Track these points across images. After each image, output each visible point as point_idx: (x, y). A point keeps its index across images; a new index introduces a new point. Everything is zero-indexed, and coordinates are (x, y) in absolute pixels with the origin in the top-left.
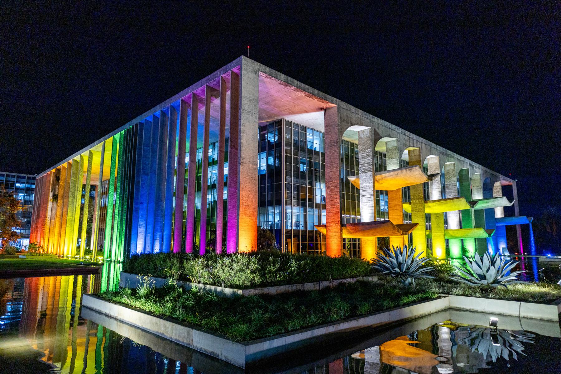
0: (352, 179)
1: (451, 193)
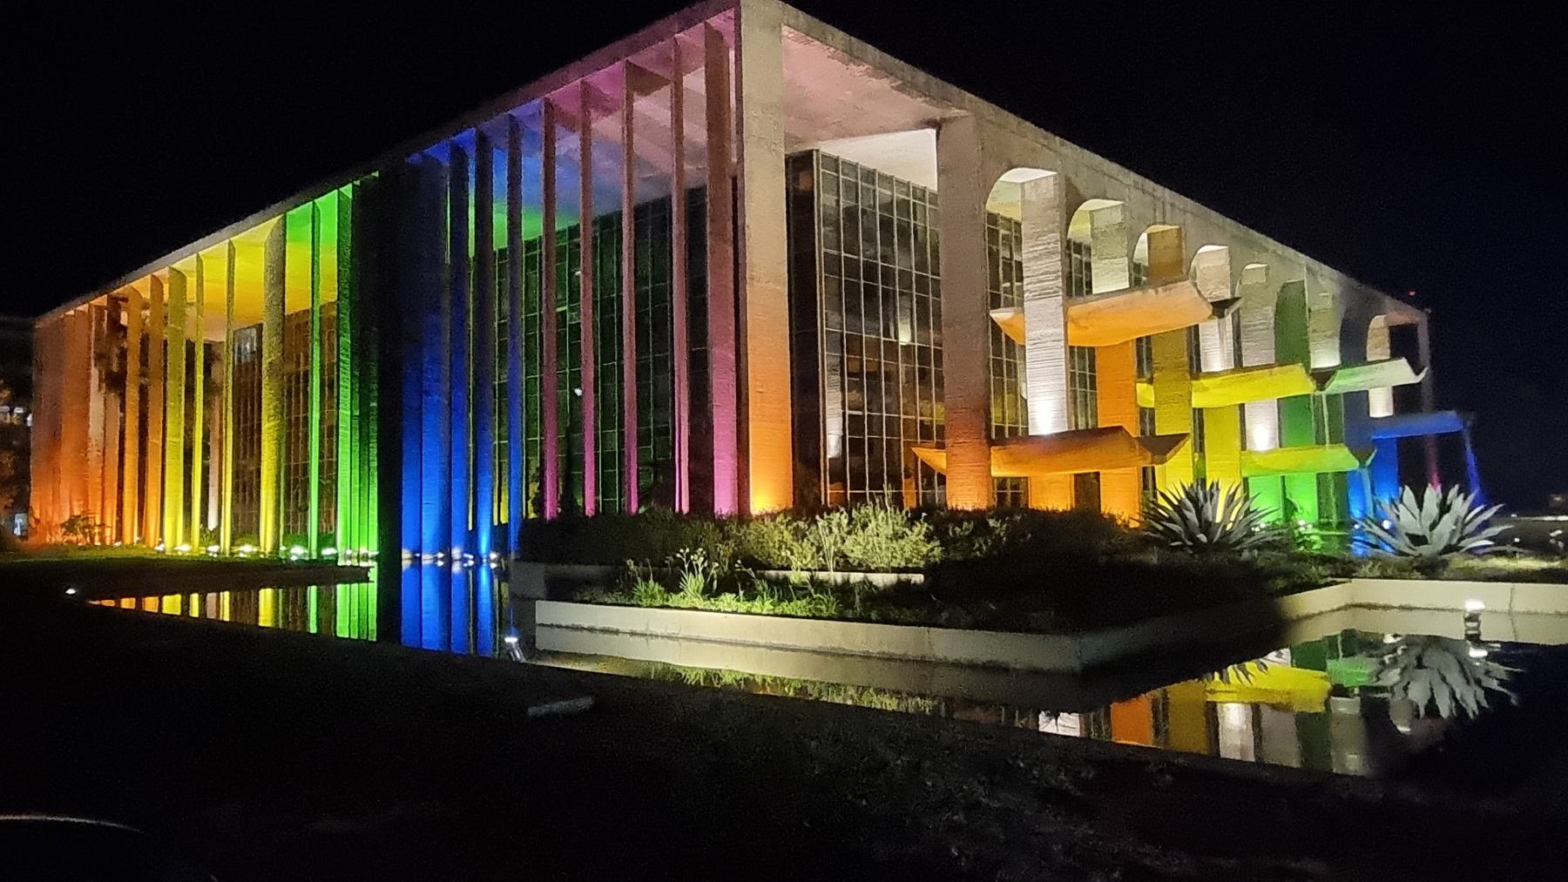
0: (1000, 315)
1: (1259, 351)
